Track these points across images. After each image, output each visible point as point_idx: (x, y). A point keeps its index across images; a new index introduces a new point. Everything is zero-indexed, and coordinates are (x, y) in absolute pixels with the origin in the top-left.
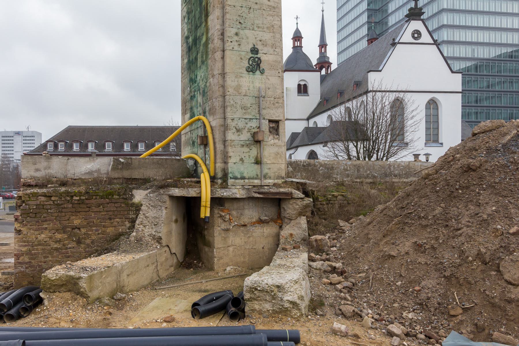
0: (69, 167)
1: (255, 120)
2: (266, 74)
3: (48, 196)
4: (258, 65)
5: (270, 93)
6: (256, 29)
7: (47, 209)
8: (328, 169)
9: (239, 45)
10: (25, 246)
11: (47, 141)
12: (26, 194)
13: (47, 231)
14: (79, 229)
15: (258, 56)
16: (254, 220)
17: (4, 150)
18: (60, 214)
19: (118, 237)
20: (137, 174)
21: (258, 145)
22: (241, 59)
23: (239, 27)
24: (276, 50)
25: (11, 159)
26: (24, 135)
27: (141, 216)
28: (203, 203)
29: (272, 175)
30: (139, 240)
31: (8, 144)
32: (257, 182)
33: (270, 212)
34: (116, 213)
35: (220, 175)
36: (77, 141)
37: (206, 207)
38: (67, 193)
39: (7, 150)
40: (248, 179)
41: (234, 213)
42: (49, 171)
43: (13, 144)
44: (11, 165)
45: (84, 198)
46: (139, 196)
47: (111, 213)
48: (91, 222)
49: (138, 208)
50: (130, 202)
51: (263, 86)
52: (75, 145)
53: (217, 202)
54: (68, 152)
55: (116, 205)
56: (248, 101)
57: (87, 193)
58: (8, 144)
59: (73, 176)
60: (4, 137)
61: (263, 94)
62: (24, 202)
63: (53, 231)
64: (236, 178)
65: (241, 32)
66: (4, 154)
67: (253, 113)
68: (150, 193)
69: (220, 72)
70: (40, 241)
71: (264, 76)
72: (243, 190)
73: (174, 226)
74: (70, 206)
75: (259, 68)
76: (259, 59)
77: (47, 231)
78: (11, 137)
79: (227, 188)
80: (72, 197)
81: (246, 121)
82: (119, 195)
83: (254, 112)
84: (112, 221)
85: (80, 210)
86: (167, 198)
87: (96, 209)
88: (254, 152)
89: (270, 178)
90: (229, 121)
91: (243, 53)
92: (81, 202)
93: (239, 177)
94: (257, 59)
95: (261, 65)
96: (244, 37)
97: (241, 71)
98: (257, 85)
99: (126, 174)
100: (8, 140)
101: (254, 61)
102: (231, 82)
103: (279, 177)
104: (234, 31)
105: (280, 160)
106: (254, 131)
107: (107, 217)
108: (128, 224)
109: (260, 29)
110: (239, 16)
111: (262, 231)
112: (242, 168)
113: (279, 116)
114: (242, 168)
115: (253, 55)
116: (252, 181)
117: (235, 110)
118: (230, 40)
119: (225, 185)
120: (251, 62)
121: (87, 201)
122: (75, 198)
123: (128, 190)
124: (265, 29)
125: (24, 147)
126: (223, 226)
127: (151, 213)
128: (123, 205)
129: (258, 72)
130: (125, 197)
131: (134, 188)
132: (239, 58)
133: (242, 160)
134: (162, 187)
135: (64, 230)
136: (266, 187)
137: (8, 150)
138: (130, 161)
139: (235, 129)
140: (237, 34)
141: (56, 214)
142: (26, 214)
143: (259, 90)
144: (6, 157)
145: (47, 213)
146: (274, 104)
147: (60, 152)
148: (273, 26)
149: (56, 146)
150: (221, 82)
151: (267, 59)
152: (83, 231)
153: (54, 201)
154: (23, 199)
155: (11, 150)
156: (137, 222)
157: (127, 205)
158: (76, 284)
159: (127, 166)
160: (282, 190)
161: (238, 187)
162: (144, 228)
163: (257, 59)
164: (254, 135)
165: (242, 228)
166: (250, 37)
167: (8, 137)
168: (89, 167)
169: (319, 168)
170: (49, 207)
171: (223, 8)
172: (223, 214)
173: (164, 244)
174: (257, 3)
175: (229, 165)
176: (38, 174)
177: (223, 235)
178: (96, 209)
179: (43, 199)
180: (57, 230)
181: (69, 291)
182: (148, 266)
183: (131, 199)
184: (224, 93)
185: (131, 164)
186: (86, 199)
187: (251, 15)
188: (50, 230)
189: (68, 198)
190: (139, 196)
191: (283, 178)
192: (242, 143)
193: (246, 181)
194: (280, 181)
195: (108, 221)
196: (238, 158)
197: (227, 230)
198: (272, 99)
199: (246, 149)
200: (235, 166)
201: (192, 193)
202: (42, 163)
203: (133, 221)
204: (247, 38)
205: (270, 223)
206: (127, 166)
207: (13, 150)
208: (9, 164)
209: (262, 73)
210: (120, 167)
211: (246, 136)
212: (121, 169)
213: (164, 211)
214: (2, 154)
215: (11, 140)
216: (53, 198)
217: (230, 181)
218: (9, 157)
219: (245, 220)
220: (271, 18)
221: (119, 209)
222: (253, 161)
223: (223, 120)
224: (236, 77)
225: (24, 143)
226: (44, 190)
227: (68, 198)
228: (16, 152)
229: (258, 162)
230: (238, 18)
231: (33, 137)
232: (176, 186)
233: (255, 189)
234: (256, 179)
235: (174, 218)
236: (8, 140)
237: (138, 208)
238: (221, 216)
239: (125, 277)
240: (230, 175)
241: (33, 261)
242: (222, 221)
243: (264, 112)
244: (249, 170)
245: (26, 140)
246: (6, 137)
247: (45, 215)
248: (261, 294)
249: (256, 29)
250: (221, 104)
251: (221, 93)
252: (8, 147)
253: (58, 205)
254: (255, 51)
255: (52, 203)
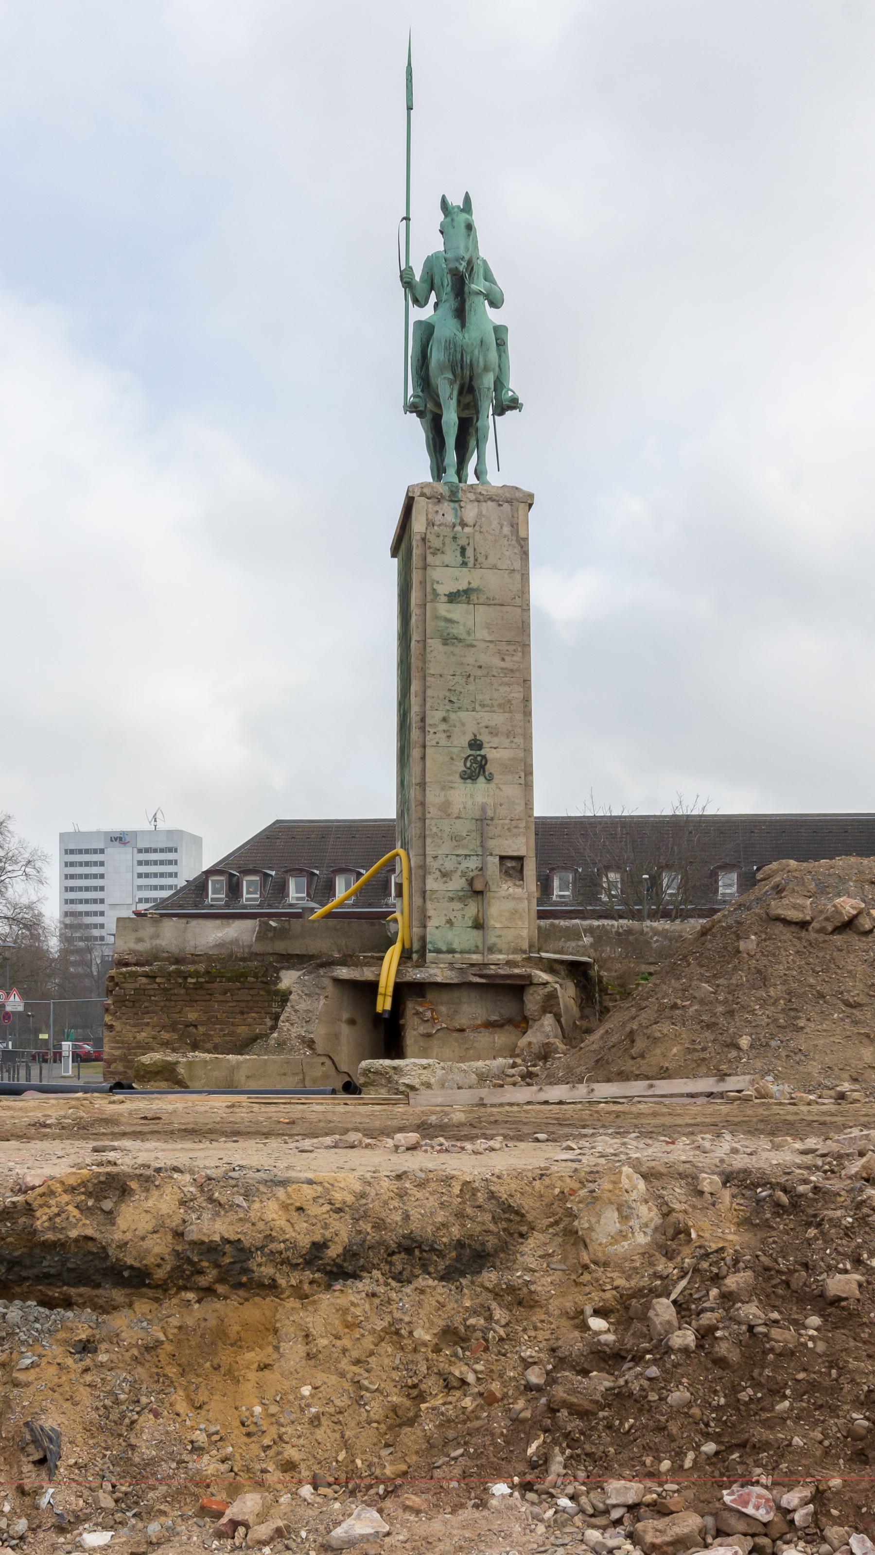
0: (189, 936)
1: (475, 858)
2: (495, 781)
3: (151, 977)
4: (482, 767)
5: (503, 812)
6: (478, 708)
7: (150, 996)
8: (670, 940)
9: (449, 737)
10: (119, 1048)
11: (209, 873)
12: (121, 974)
13: (150, 1028)
14: (195, 1026)
15: (482, 752)
16: (479, 1022)
17: (72, 902)
18: (167, 1003)
19: (254, 1039)
20: (297, 948)
21: (480, 897)
22: (452, 759)
23: (448, 708)
24: (515, 740)
25: (96, 933)
26: (142, 845)
27: (288, 1009)
28: (381, 990)
29: (504, 947)
30: (281, 1044)
31: (87, 876)
32: (476, 958)
33: (505, 1008)
34: (251, 1004)
35: (416, 946)
36: (299, 872)
37: (385, 995)
38: (179, 973)
39: (81, 901)
40: (461, 952)
41: (443, 1009)
42: (158, 942)
43: (102, 876)
44: (96, 953)
45: (202, 980)
46: (288, 979)
47: (243, 1004)
48: (213, 1017)
49: (284, 997)
50: (273, 988)
51: (490, 801)
52: (292, 884)
53: (402, 990)
54: (270, 906)
55: (251, 992)
56: (463, 827)
57: (208, 973)
58: (87, 876)
59: (193, 951)
60: (72, 852)
61: (490, 813)
62: (117, 984)
63: (158, 1029)
64: (438, 951)
65: (453, 716)
66: (72, 914)
67: (471, 847)
68: (304, 975)
69: (418, 780)
70: (139, 1042)
71: (492, 785)
72: (451, 970)
73: (345, 1029)
74: (183, 991)
75: (484, 772)
76: (484, 757)
77: (150, 1028)
78: (95, 851)
79: (423, 966)
80: (185, 978)
81: (459, 859)
82: (256, 977)
83: (473, 844)
84: (245, 1016)
85: (198, 998)
86: (327, 982)
87: (222, 998)
88: (472, 909)
89: (500, 952)
90: (429, 860)
91: (455, 750)
92: (198, 986)
93: (444, 949)
94: (479, 758)
95: (487, 767)
96: (458, 724)
97: (450, 778)
98: (480, 799)
99: (280, 947)
100: (87, 864)
101: (475, 760)
102: (433, 797)
103: (516, 951)
104: (440, 714)
105: (520, 923)
106: (472, 874)
107: (237, 1010)
108: (269, 1022)
109: (487, 709)
110: (449, 690)
111: (490, 1039)
112: (450, 935)
113: (519, 850)
114: (450, 935)
115: (473, 752)
116: (467, 956)
117: (440, 841)
118: (432, 731)
119: (422, 963)
120: (468, 764)
121: (208, 986)
122: (190, 980)
123: (271, 971)
124: (495, 708)
125: (140, 888)
126: (422, 1029)
127: (303, 1005)
128: (262, 993)
129: (481, 779)
130: (264, 980)
131: (283, 968)
132: (447, 759)
133: (450, 922)
134: (322, 965)
135: (173, 1027)
136: (492, 967)
137: (87, 901)
138: (286, 925)
139: (438, 873)
140: (444, 720)
141: (162, 1004)
142: (120, 1002)
143: (483, 808)
144: (80, 926)
145: (150, 1001)
146: (509, 830)
147: (245, 907)
148: (509, 701)
149: (234, 889)
150: (419, 797)
151: (498, 756)
152: (201, 1029)
153: (159, 984)
154: (116, 980)
155: (95, 901)
156: (282, 1018)
157: (269, 992)
158: (173, 1071)
159: (281, 934)
160: (517, 971)
161: (442, 966)
162: (291, 1026)
163: (479, 758)
164: (471, 882)
165: (455, 1034)
166: (469, 723)
167: (87, 851)
168: (220, 935)
169: (651, 938)
170: (152, 992)
171: (424, 678)
172: (421, 1010)
173: (320, 1050)
174: (480, 667)
175: (428, 929)
176: (140, 947)
177: (422, 1044)
178: (222, 998)
179: (144, 980)
180: (164, 1027)
181: (166, 1080)
182: (285, 1074)
183: (276, 984)
184: (424, 814)
185: (289, 930)
186: (206, 982)
187: (471, 687)
188: (153, 1027)
189: (180, 981)
190: (288, 979)
191: (524, 952)
192: (450, 894)
193: (457, 956)
194: (518, 957)
195: (239, 1016)
196: (443, 920)
197: (429, 1036)
198: (507, 821)
199: (457, 905)
200: (437, 931)
201: (367, 974)
202: (147, 930)
203: (276, 1018)
204: (463, 725)
205: (506, 1027)
206: (281, 934)
207: (102, 901)
208: (90, 950)
209: (489, 779)
210: (270, 935)
211: (457, 884)
212: (272, 939)
213: (323, 1001)
214: (66, 914)
215: (95, 864)
216: (158, 980)
217: (430, 956)
218: (88, 926)
219: (462, 1020)
220: (507, 689)
221: (255, 998)
222: (470, 924)
223: (422, 858)
224: (443, 789)
225: (140, 876)
226: (147, 968)
227: (180, 981)
228: (113, 906)
229: (479, 925)
230: (448, 694)
231: (170, 850)
232: (343, 963)
233: (474, 970)
234: (475, 953)
235: (345, 1016)
236: (87, 864)
237: (284, 997)
238: (417, 1013)
239: (243, 1079)
240: (429, 946)
241: (129, 1071)
242: (419, 1021)
243: (491, 843)
244: (462, 937)
245: (147, 863)
246: (80, 852)
247: (146, 1004)
248: (376, 1078)
249: (478, 708)
250: (418, 832)
251: (420, 815)
252: (87, 889)
253: (165, 989)
254: (476, 744)
255: (156, 986)
